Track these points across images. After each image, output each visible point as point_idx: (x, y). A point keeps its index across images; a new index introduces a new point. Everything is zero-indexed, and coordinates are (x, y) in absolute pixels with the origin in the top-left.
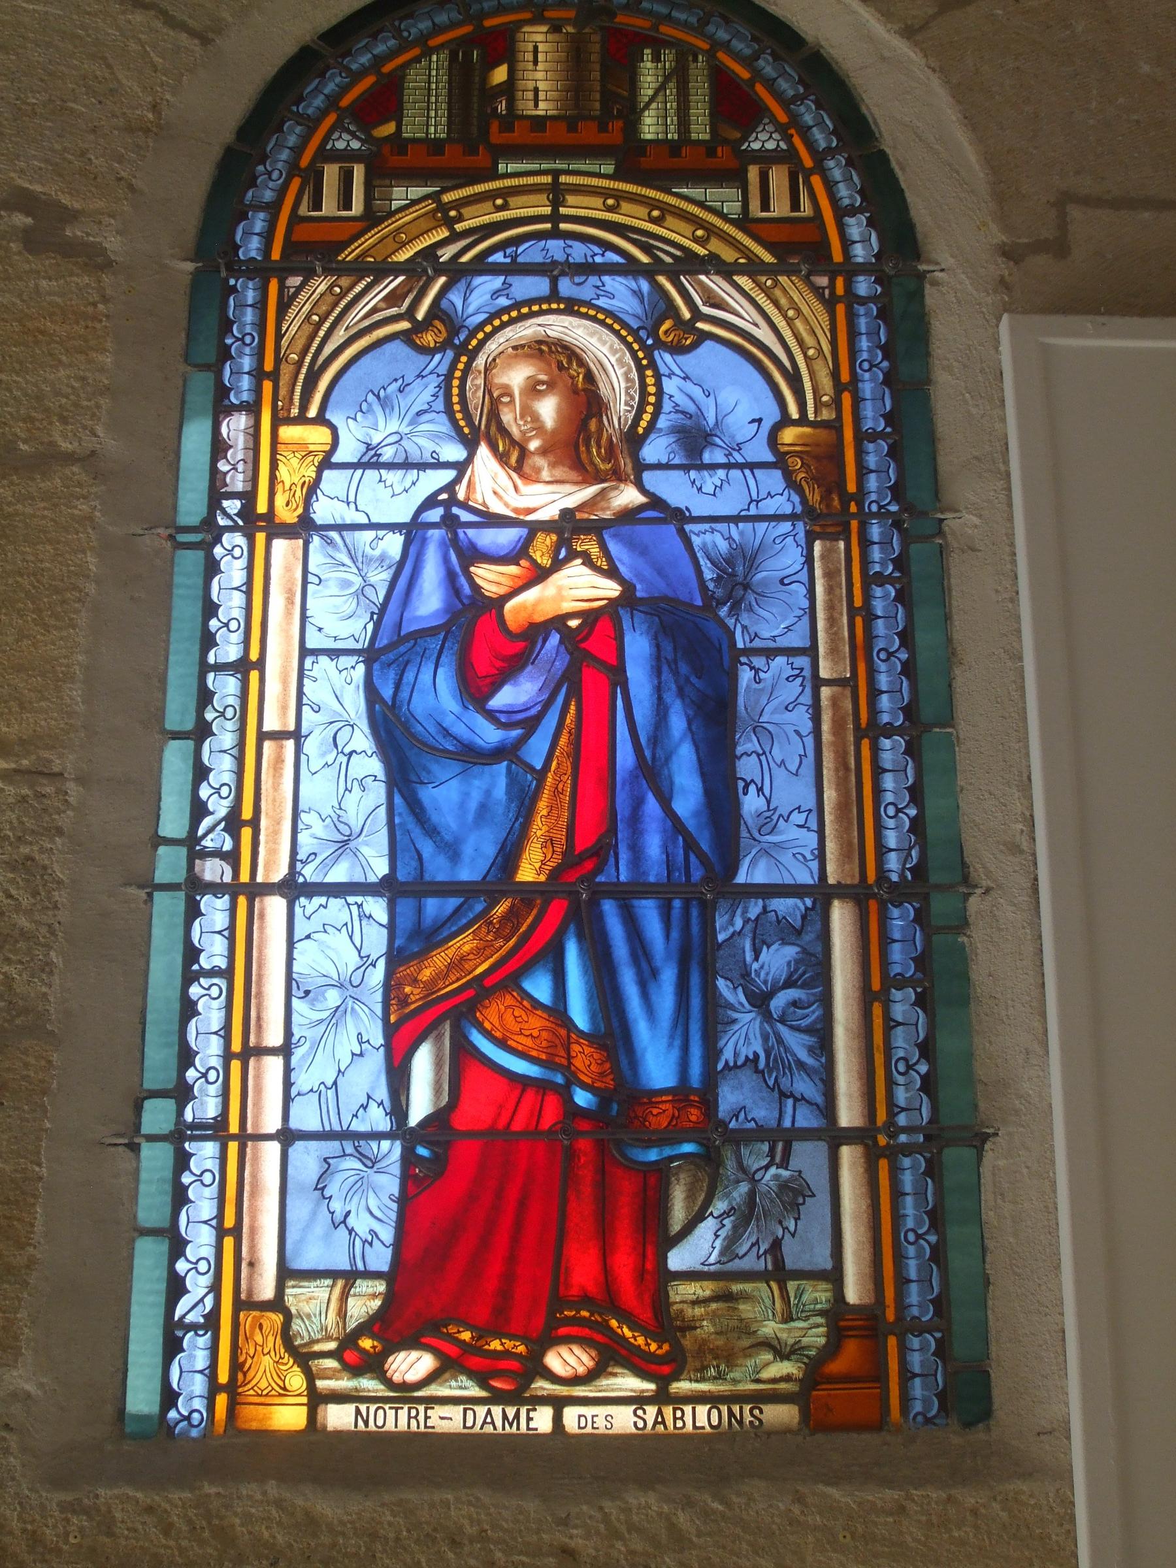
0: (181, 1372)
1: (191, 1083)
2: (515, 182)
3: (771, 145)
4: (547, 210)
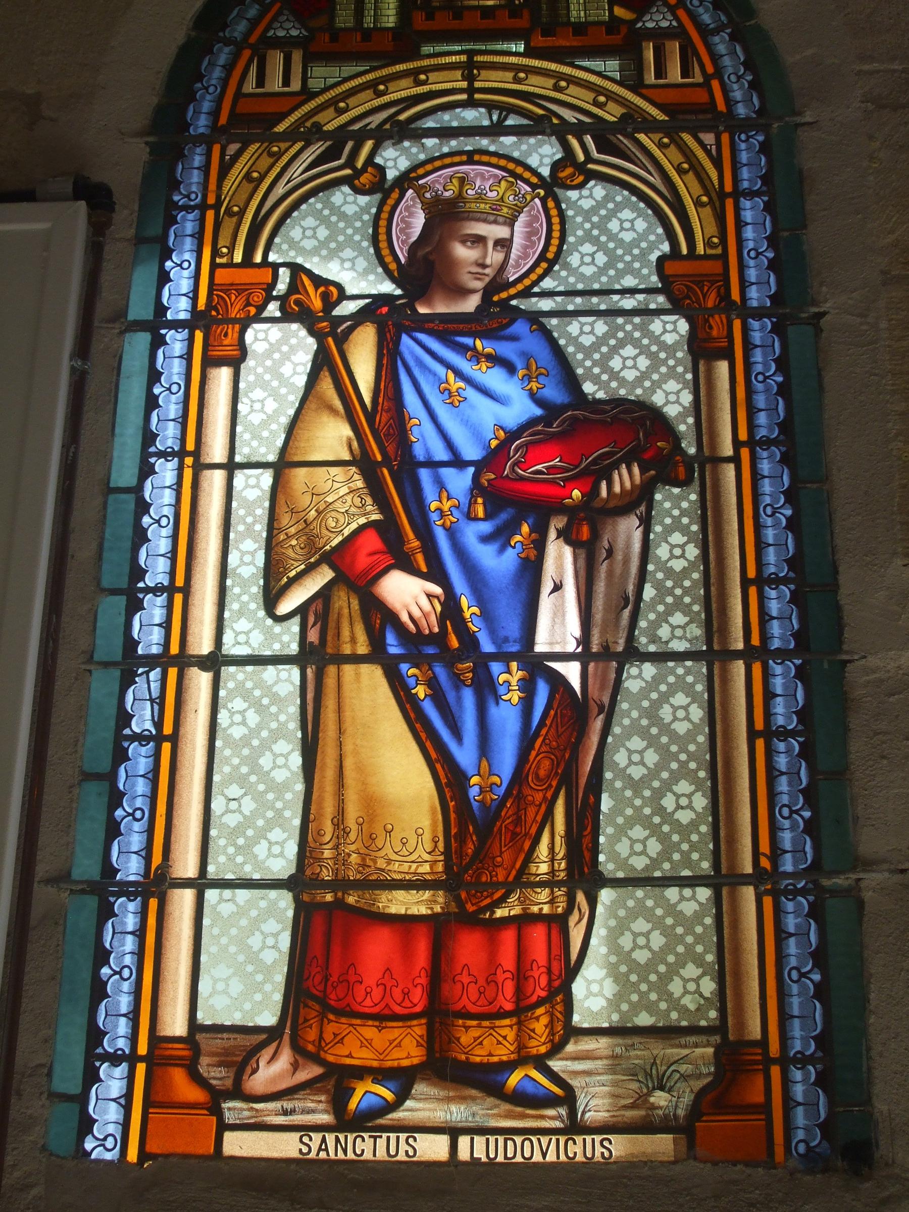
0: (141, 625)
1: (105, 979)
2: (433, 61)
3: (665, 24)
4: (464, 84)
